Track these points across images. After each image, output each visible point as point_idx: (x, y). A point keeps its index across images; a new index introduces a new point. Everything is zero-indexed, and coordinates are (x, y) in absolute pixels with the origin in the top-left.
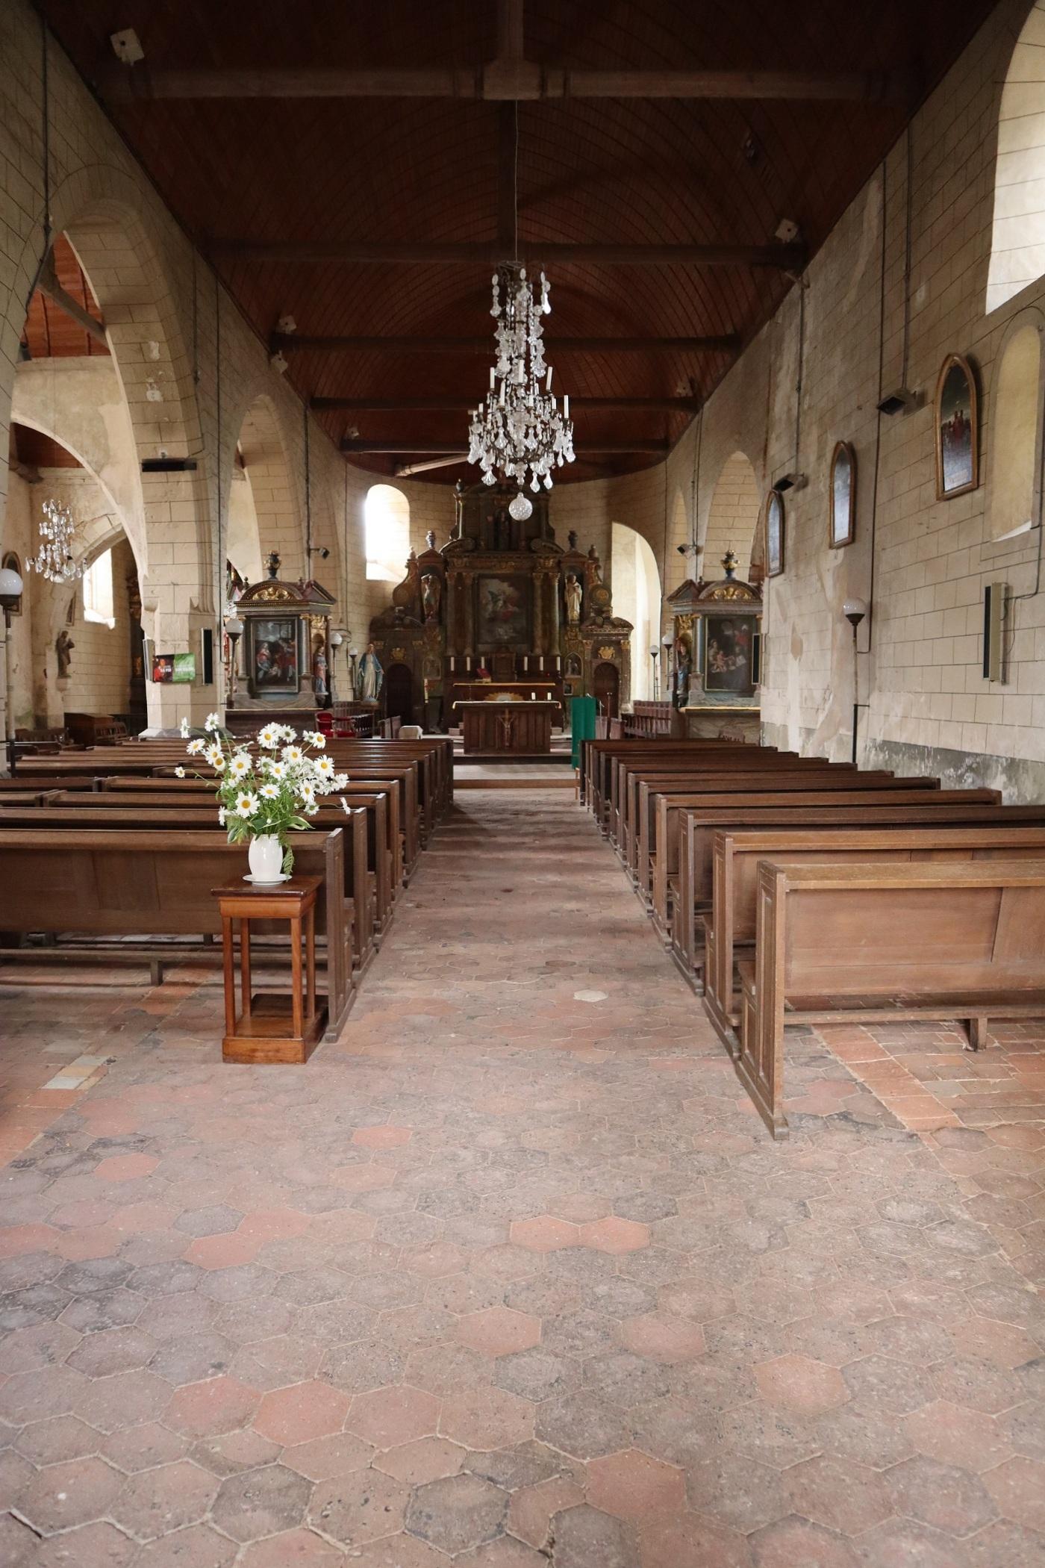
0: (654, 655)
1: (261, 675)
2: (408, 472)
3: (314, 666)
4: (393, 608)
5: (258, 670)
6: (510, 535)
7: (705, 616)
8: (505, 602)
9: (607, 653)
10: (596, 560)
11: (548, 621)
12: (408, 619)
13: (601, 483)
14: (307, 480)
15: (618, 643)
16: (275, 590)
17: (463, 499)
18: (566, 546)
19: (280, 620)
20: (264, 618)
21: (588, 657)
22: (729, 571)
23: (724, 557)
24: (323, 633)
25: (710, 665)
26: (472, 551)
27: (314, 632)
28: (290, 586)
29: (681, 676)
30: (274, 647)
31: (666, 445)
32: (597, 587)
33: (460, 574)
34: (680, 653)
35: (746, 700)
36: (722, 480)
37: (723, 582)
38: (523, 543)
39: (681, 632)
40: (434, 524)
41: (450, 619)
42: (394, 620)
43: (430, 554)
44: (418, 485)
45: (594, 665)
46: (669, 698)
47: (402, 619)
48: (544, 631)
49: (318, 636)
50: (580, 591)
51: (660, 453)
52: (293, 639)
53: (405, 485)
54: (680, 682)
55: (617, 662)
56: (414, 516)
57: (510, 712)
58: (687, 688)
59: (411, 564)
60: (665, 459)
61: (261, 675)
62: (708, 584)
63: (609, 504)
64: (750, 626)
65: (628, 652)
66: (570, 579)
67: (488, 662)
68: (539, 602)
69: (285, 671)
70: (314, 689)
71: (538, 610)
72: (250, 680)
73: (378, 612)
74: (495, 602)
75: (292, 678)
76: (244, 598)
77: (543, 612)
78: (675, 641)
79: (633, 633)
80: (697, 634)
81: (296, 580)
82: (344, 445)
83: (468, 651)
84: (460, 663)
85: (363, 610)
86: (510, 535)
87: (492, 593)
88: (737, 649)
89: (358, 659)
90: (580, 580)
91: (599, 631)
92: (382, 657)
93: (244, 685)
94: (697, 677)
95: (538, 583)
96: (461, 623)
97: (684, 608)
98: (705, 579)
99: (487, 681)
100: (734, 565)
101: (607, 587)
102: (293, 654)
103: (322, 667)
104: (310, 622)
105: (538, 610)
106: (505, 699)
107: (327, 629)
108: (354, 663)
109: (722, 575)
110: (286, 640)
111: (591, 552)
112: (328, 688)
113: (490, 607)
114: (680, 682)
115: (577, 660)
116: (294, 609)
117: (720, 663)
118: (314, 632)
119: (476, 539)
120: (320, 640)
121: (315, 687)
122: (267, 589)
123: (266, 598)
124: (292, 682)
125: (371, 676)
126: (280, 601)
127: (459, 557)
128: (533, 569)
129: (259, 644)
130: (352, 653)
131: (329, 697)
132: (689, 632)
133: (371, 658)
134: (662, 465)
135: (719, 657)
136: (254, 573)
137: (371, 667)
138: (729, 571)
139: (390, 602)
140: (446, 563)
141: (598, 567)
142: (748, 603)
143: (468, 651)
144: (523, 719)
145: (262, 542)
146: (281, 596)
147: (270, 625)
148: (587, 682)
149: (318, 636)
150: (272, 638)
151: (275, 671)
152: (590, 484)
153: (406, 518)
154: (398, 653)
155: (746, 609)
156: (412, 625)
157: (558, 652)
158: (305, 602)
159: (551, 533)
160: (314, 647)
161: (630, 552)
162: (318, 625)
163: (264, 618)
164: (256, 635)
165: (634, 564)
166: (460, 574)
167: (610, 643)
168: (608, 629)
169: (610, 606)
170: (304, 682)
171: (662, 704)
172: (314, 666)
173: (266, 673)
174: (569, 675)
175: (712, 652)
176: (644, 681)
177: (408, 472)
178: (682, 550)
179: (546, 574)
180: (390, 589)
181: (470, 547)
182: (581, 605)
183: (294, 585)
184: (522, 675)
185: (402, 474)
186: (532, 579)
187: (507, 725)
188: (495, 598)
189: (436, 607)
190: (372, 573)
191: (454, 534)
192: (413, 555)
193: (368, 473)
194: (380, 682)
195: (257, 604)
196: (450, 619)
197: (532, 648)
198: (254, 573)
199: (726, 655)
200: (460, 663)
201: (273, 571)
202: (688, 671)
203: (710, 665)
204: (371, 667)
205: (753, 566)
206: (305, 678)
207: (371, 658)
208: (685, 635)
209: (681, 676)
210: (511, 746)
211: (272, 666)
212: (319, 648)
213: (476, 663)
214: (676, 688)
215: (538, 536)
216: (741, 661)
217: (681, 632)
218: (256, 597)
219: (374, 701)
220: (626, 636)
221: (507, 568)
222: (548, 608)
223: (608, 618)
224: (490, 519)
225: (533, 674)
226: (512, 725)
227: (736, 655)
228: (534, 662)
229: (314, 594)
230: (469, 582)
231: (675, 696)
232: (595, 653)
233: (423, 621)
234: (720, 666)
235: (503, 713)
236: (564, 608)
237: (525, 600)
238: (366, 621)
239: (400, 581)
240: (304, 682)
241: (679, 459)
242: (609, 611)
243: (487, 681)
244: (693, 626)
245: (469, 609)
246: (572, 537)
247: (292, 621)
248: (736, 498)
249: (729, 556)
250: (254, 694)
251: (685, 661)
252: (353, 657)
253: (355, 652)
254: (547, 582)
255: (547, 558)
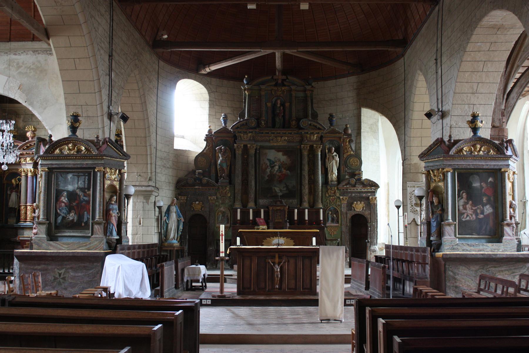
0: (398, 207)
1: (60, 219)
2: (208, 70)
3: (107, 214)
4: (194, 172)
5: (57, 215)
6: (284, 116)
7: (454, 170)
8: (279, 167)
9: (359, 207)
10: (350, 136)
11: (313, 182)
12: (205, 180)
13: (353, 79)
14: (111, 56)
15: (368, 198)
16: (74, 145)
17: (248, 90)
18: (326, 126)
19: (79, 171)
20: (64, 170)
21: (344, 210)
22: (475, 130)
23: (470, 118)
24: (117, 184)
25: (461, 214)
26: (255, 128)
27: (108, 183)
28: (88, 142)
29: (434, 224)
30: (72, 195)
31: (404, 43)
32: (351, 156)
33: (245, 146)
34: (432, 203)
35: (495, 245)
36: (467, 57)
37: (470, 140)
38: (294, 123)
39: (433, 185)
40: (228, 111)
41: (238, 180)
42: (194, 180)
43: (223, 131)
44: (214, 81)
45: (349, 216)
46: (421, 242)
47: (201, 180)
48: (310, 189)
49: (112, 187)
50: (338, 159)
51: (399, 50)
52: (89, 189)
53: (206, 80)
54: (434, 230)
55: (366, 213)
56: (212, 103)
57: (280, 257)
58: (440, 234)
59: (209, 138)
60: (403, 55)
61: (60, 219)
62: (456, 142)
63: (358, 94)
64: (495, 179)
65: (375, 205)
66: (330, 150)
67: (266, 213)
68: (306, 168)
69: (80, 217)
70: (105, 233)
71: (306, 173)
72: (50, 224)
73: (182, 174)
74: (272, 167)
75: (87, 223)
76: (46, 152)
77: (309, 175)
78: (428, 193)
79: (379, 190)
80: (449, 186)
81: (93, 138)
82: (156, 44)
83: (251, 204)
84: (245, 213)
85: (170, 172)
86: (284, 116)
87: (269, 160)
88: (485, 199)
89: (164, 209)
90: (338, 151)
91: (352, 189)
92: (183, 209)
93: (43, 228)
94: (449, 225)
95: (305, 153)
96: (245, 183)
97: (436, 162)
98: (454, 138)
99: (263, 228)
100: (479, 124)
101: (358, 155)
102: (88, 202)
103: (114, 214)
104: (104, 174)
105: (306, 173)
106: (278, 243)
107: (121, 181)
108: (160, 212)
109: (468, 134)
110: (82, 189)
111: (346, 129)
112: (119, 233)
113: (268, 170)
114: (434, 230)
115: (336, 212)
116: (90, 162)
117: (470, 212)
118: (108, 183)
119: (258, 119)
120: (113, 190)
121: (106, 231)
122: (67, 144)
123: (66, 152)
124: (86, 227)
125: (173, 222)
126: (79, 155)
127: (245, 133)
128: (301, 142)
129: (59, 193)
130: (158, 204)
131: (119, 241)
132: (441, 184)
133: (174, 209)
134: (402, 59)
135: (468, 206)
136: (59, 131)
137: (174, 216)
138: (475, 130)
139: (192, 166)
140: (235, 137)
141: (350, 141)
142: (493, 158)
143: (251, 204)
144: (292, 261)
145: (67, 105)
146: (79, 151)
147: (70, 176)
148: (344, 229)
149: (112, 187)
150: (70, 188)
151: (72, 216)
152: (344, 80)
153: (206, 105)
154: (197, 206)
155: (492, 164)
156: (208, 184)
157: (321, 206)
158: (100, 156)
159: (315, 116)
160: (107, 196)
161: (374, 130)
162: (112, 177)
163: (64, 170)
164: (57, 185)
165: (377, 139)
166: (245, 146)
167: (361, 199)
168: (359, 188)
169: (360, 169)
170: (96, 227)
171: (417, 249)
172: (107, 214)
173: (64, 218)
174: (329, 224)
175: (462, 202)
176: (390, 229)
177: (208, 70)
178: (429, 115)
179: (312, 147)
180: (193, 157)
181: (253, 125)
182: (339, 170)
183: (92, 142)
184: (292, 224)
185: (203, 72)
186: (301, 150)
187: (277, 269)
188: (272, 164)
189: (227, 172)
190: (178, 144)
191: (242, 115)
192: (210, 131)
193: (177, 70)
194: (181, 227)
195: (58, 158)
196: (238, 180)
197: (301, 202)
198: (59, 131)
199: (474, 204)
200: (245, 213)
201: (73, 128)
202: (442, 218)
203: (461, 214)
204: (174, 216)
205: (493, 127)
206: (98, 223)
207: (174, 209)
208: (436, 187)
209: (434, 224)
210: (280, 288)
211: (69, 212)
212: (112, 197)
213: (257, 214)
214: (429, 234)
215: (306, 116)
216: (488, 210)
217: (433, 185)
218: (57, 151)
219: (176, 243)
220: (374, 193)
221: (281, 142)
222: (313, 172)
223: (360, 179)
224: (269, 104)
225: (301, 222)
226: (281, 269)
227: (484, 205)
228: (301, 214)
229: (112, 150)
230: (252, 152)
231: (429, 243)
232: (350, 206)
233: (217, 181)
234: (469, 215)
235: (273, 257)
236: (326, 172)
237: (294, 167)
238: (173, 181)
239: (200, 151)
240: (96, 227)
241: (420, 50)
242: (360, 174)
243: (263, 228)
244: (445, 179)
245: (252, 172)
246: (331, 118)
247: (89, 173)
248: (481, 64)
249: (475, 117)
250: (52, 237)
251: (438, 212)
252: (160, 208)
253: (161, 204)
254: (312, 151)
255: (313, 134)
